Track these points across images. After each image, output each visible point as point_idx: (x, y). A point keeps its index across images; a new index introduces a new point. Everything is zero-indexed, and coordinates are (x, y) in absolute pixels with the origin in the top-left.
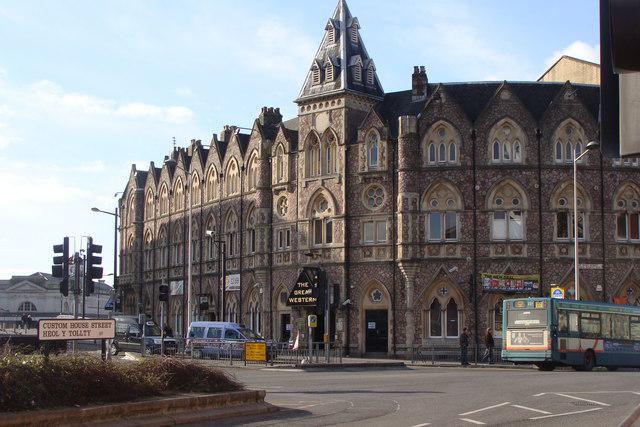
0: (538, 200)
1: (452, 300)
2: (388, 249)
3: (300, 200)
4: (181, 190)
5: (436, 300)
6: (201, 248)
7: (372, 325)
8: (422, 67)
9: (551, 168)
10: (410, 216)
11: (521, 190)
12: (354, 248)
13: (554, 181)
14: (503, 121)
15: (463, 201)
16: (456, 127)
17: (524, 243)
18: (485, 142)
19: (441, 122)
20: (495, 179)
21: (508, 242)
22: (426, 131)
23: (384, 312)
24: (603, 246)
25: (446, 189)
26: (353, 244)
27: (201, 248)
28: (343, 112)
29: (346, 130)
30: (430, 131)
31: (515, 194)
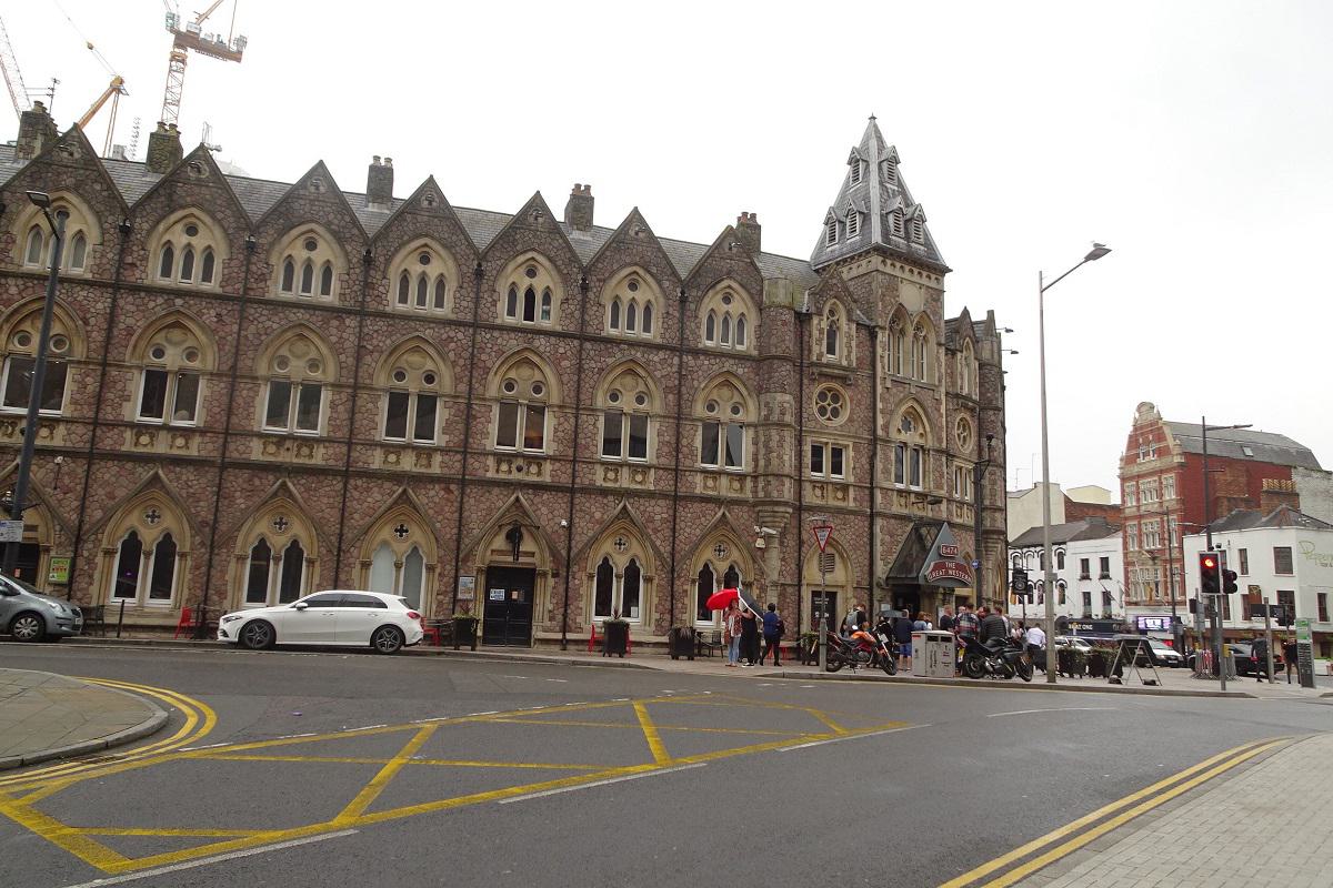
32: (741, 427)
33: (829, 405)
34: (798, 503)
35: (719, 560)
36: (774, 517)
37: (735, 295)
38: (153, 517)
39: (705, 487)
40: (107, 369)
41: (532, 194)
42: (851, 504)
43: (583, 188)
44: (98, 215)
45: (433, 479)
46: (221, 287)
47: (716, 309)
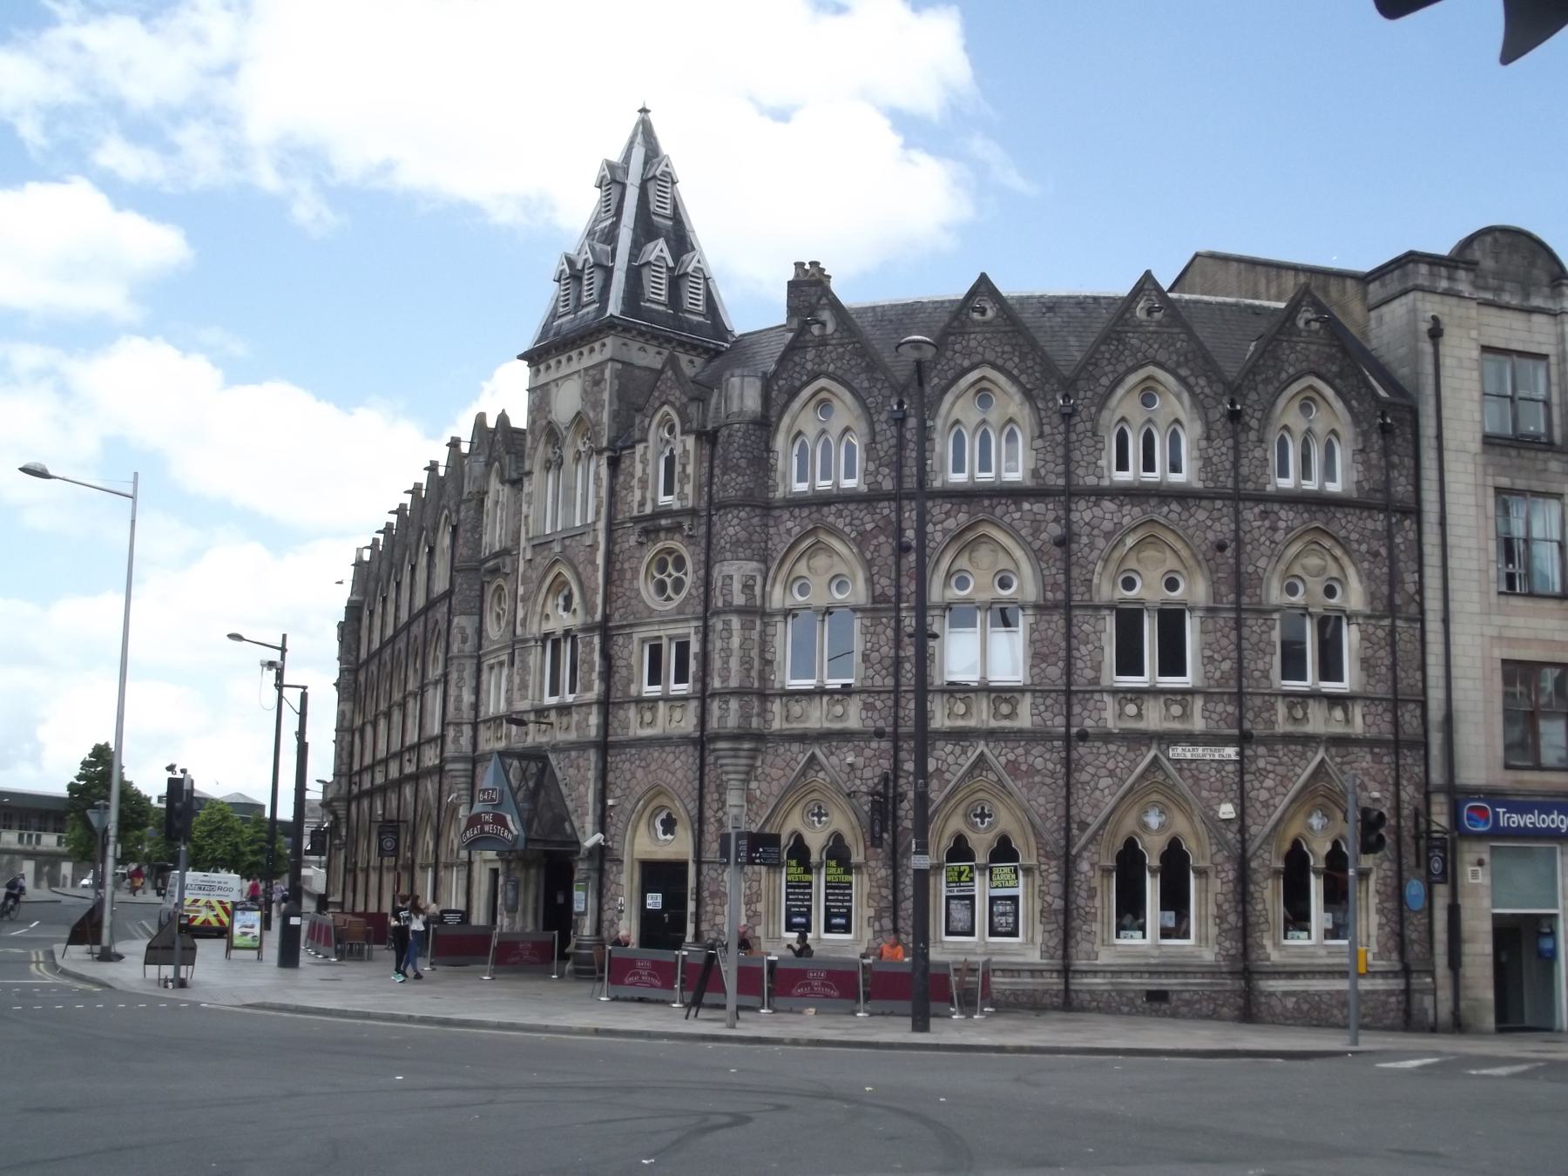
0: (1061, 578)
1: (838, 838)
5: (1131, 844)
7: (654, 901)
8: (814, 264)
9: (1099, 494)
11: (1018, 553)
12: (620, 705)
13: (1107, 526)
14: (974, 376)
15: (870, 581)
16: (854, 393)
17: (1021, 690)
19: (823, 382)
20: (951, 523)
21: (985, 689)
23: (678, 868)
24: (1239, 697)
25: (831, 551)
26: (617, 695)
30: (796, 404)
31: (1004, 563)
32: (1303, 615)
33: (670, 576)
36: (736, 757)
38: (819, 815)
39: (1121, 715)
40: (1244, 616)
43: (807, 267)
44: (1028, 395)
45: (845, 736)
47: (1128, 417)
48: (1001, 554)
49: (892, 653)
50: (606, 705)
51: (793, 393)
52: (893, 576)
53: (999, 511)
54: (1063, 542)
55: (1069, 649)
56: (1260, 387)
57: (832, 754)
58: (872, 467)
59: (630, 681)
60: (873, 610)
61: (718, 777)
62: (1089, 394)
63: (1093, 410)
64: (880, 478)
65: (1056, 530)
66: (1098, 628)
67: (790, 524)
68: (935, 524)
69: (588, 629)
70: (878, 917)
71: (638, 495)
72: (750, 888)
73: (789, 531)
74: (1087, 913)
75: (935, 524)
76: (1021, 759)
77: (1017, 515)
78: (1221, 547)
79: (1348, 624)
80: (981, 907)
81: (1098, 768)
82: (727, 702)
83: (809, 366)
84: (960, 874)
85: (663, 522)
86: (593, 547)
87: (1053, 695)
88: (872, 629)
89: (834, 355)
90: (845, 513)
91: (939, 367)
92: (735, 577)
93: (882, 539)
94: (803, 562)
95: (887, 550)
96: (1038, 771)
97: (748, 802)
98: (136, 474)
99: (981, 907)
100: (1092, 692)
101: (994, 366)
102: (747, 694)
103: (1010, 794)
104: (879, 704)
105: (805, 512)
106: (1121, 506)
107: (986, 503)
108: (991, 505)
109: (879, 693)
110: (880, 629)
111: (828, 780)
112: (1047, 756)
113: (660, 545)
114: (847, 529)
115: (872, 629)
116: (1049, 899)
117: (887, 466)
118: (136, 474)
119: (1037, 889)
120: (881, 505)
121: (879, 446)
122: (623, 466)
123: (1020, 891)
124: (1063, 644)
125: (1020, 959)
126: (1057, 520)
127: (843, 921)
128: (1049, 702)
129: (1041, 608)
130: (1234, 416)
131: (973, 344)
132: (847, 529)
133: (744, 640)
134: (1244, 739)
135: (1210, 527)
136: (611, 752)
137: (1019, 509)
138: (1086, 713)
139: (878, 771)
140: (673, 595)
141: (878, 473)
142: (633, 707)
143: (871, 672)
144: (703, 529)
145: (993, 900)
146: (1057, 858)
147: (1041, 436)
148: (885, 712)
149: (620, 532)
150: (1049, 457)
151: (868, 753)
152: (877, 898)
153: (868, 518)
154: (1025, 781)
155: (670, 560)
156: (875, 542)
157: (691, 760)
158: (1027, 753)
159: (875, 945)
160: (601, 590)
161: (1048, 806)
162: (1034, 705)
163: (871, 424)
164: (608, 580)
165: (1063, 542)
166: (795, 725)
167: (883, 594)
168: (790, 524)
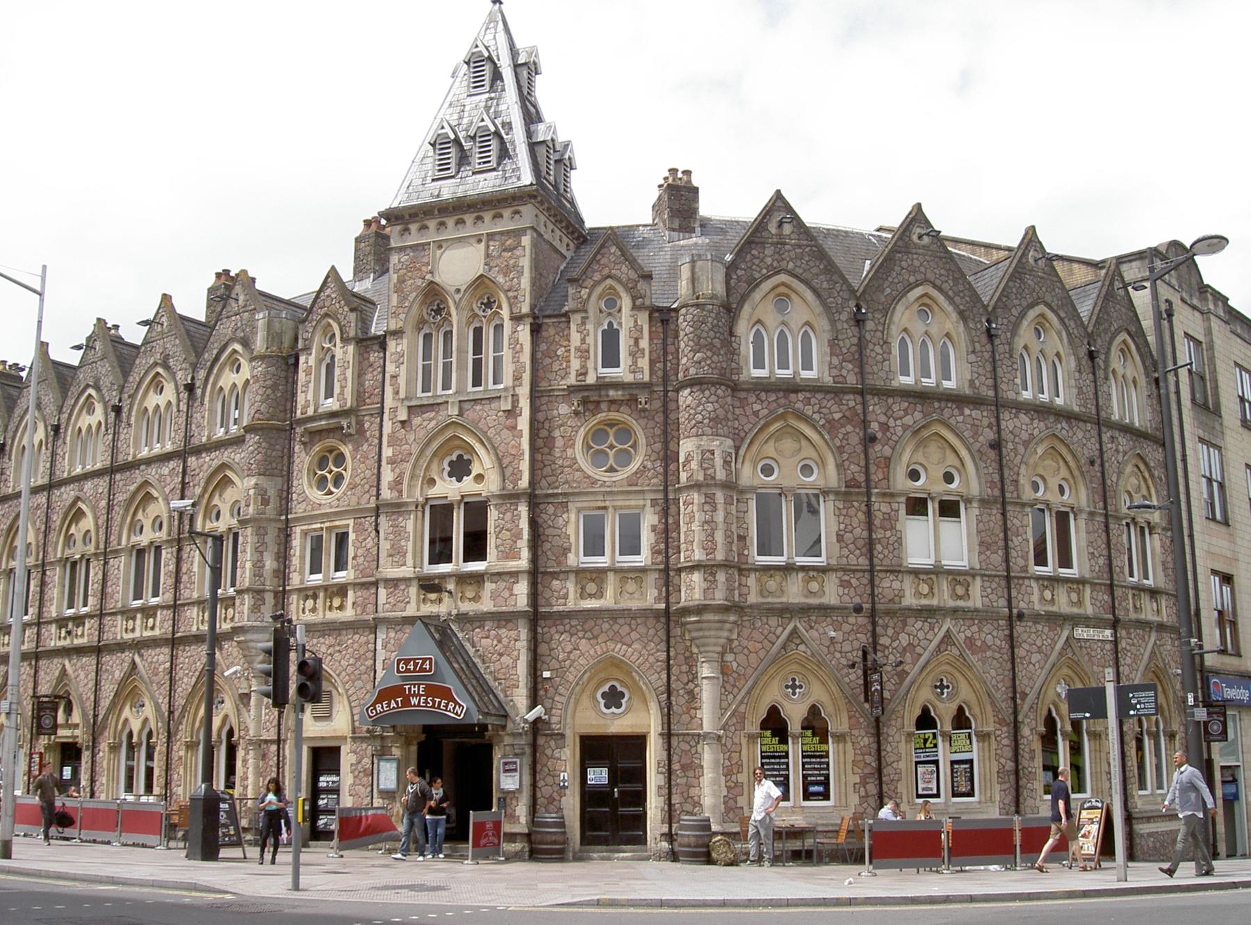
1: (814, 711)
2: (652, 578)
3: (387, 452)
4: (40, 434)
6: (43, 584)
7: (598, 776)
10: (720, 497)
11: (964, 453)
12: (555, 575)
13: (1025, 436)
14: (918, 291)
15: (839, 466)
17: (972, 574)
18: (885, 327)
19: (783, 277)
20: (908, 420)
21: (937, 571)
22: (744, 298)
23: (636, 743)
27: (43, 584)
28: (526, 240)
29: (534, 283)
30: (757, 295)
33: (330, 472)
34: (1111, 616)
35: (942, 701)
37: (793, 296)
41: (770, 193)
42: (1089, 610)
44: (962, 315)
45: (825, 610)
46: (630, 372)
48: (949, 452)
49: (865, 534)
50: (536, 575)
51: (754, 284)
52: (862, 463)
53: (947, 413)
54: (997, 445)
55: (1006, 539)
56: (1103, 335)
57: (812, 628)
58: (835, 361)
59: (566, 551)
60: (846, 493)
61: (687, 649)
62: (1005, 321)
63: (1009, 335)
64: (844, 372)
65: (990, 435)
66: (1024, 523)
67: (757, 407)
68: (895, 420)
69: (510, 498)
70: (863, 783)
71: (575, 364)
72: (729, 759)
73: (756, 413)
74: (1030, 772)
75: (895, 420)
76: (976, 635)
77: (960, 419)
78: (1092, 463)
79: (1150, 534)
80: (944, 768)
81: (1031, 645)
82: (713, 574)
83: (769, 261)
84: (925, 741)
85: (612, 393)
86: (512, 413)
87: (997, 579)
88: (844, 511)
89: (793, 254)
90: (813, 401)
91: (890, 279)
92: (716, 453)
93: (849, 428)
94: (771, 443)
95: (855, 439)
96: (989, 647)
97: (723, 673)
98: (44, 267)
99: (944, 768)
100: (1024, 578)
101: (935, 286)
102: (731, 567)
103: (970, 667)
104: (854, 581)
105: (773, 397)
106: (1032, 420)
107: (936, 405)
108: (939, 407)
109: (854, 571)
110: (852, 512)
111: (809, 653)
112: (995, 633)
113: (601, 416)
114: (816, 416)
115: (844, 511)
116: (1003, 761)
117: (850, 362)
118: (44, 267)
119: (993, 753)
120: (847, 397)
121: (841, 343)
122: (544, 334)
123: (974, 756)
124: (1002, 535)
125: (985, 817)
126: (990, 426)
127: (821, 789)
128: (994, 585)
129: (984, 502)
130: (1092, 356)
131: (916, 263)
132: (816, 416)
133: (727, 514)
134: (1115, 624)
135: (1085, 445)
136: (542, 623)
137: (962, 414)
138: (1020, 597)
139: (856, 645)
140: (333, 489)
141: (842, 368)
142: (572, 577)
143: (846, 552)
144: (657, 404)
145: (953, 763)
146: (1008, 725)
147: (973, 352)
148: (860, 590)
149: (544, 400)
150: (981, 371)
151: (846, 627)
152: (862, 764)
153: (835, 408)
154: (980, 655)
155: (331, 458)
156: (843, 430)
157: (652, 632)
158: (980, 630)
159: (862, 810)
160: (527, 457)
161: (999, 678)
162: (983, 588)
163: (833, 322)
164: (534, 449)
165: (997, 445)
166: (770, 600)
167: (854, 479)
168: (757, 407)
